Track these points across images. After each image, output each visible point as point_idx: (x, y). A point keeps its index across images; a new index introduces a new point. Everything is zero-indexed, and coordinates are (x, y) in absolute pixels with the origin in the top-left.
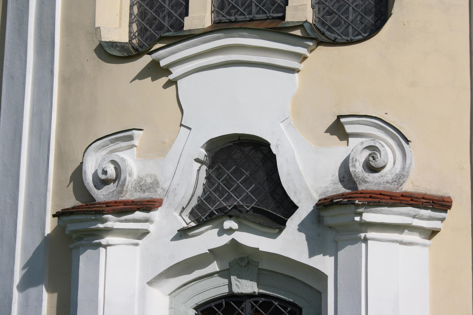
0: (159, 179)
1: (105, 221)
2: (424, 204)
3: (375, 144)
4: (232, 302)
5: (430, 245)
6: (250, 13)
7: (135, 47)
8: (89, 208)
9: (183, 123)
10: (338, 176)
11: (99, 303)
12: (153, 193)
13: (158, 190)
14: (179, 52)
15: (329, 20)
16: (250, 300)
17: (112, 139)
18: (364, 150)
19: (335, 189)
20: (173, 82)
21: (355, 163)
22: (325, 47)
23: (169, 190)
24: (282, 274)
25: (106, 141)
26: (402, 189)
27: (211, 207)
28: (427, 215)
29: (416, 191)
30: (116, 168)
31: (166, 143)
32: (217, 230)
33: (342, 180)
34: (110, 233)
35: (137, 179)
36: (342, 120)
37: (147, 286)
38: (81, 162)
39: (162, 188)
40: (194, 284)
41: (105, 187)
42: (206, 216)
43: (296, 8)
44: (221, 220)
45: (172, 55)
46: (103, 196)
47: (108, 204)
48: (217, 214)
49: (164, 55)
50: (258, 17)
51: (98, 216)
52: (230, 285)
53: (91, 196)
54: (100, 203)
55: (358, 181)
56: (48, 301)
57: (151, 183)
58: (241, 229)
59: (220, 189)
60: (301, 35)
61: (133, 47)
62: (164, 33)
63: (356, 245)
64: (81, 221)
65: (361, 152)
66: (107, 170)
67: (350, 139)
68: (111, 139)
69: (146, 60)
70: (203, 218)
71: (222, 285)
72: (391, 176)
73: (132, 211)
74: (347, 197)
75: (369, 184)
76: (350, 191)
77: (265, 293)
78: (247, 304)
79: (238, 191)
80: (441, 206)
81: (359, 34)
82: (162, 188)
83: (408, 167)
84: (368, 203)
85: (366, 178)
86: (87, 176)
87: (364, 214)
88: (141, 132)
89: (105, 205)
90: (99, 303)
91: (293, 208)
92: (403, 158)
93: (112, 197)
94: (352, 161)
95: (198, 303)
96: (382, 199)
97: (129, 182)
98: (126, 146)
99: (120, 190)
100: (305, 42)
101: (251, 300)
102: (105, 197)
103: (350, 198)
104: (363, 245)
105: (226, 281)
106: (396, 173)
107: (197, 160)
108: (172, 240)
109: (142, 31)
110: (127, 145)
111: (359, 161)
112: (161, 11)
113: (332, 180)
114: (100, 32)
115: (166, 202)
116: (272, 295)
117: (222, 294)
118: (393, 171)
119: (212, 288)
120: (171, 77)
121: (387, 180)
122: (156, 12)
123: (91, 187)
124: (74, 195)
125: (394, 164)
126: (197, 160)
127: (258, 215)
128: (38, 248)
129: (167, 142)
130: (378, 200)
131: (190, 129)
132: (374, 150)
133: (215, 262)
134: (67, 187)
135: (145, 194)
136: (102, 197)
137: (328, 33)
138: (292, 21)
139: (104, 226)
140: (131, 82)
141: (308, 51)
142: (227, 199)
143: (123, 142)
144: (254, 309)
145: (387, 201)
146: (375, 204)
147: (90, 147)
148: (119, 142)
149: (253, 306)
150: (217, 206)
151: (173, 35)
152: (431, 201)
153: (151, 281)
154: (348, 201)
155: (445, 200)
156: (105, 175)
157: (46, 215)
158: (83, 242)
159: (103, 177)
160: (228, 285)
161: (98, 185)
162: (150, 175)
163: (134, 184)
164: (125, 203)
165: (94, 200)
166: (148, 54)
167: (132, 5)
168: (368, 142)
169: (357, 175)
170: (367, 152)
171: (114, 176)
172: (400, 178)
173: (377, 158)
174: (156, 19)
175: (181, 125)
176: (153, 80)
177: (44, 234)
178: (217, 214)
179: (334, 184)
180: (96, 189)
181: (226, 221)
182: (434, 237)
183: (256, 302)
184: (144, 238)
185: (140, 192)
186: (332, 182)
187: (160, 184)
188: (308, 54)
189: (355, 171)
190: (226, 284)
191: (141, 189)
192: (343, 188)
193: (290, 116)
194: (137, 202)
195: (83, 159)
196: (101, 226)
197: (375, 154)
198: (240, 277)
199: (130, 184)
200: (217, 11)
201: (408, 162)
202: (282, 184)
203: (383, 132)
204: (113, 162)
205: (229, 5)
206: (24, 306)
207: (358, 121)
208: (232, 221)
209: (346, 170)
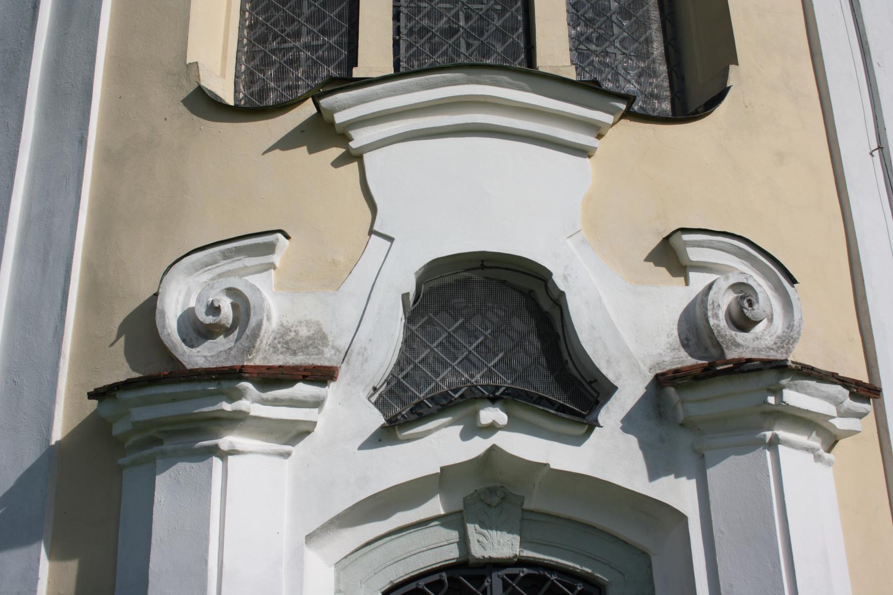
0: (326, 330)
1: (240, 395)
3: (747, 281)
4: (463, 577)
9: (376, 228)
10: (678, 336)
11: (209, 578)
13: (326, 350)
14: (375, 100)
16: (500, 573)
17: (229, 249)
19: (677, 358)
21: (717, 311)
22: (632, 122)
23: (351, 350)
24: (569, 520)
25: (215, 253)
31: (339, 264)
33: (685, 343)
34: (238, 426)
35: (279, 329)
38: (154, 292)
39: (333, 347)
40: (387, 542)
41: (206, 343)
45: (359, 104)
46: (203, 359)
49: (346, 102)
51: (225, 385)
52: (464, 543)
55: (725, 343)
56: (49, 582)
57: (309, 338)
58: (514, 425)
63: (750, 455)
64: (174, 399)
66: (219, 306)
67: (692, 275)
68: (225, 250)
71: (446, 543)
72: (771, 339)
74: (679, 379)
75: (743, 349)
77: (535, 558)
78: (495, 582)
80: (868, 390)
82: (335, 346)
83: (798, 325)
84: (801, 367)
86: (167, 321)
90: (209, 578)
92: (784, 310)
93: (227, 359)
94: (712, 307)
95: (394, 580)
97: (265, 333)
98: (256, 265)
99: (247, 347)
100: (613, 103)
101: (503, 573)
102: (210, 361)
105: (454, 535)
106: (777, 334)
108: (362, 447)
113: (669, 343)
114: (198, 71)
115: (346, 372)
116: (548, 562)
117: (446, 561)
119: (424, 549)
121: (766, 345)
123: (175, 341)
128: (30, 473)
129: (342, 261)
131: (391, 239)
134: (112, 345)
135: (297, 358)
139: (232, 408)
143: (250, 256)
144: (510, 589)
147: (177, 264)
148: (242, 257)
150: (430, 392)
156: (213, 316)
157: (55, 404)
159: (209, 320)
160: (458, 543)
161: (191, 339)
162: (307, 321)
163: (271, 338)
172: (788, 343)
175: (372, 232)
179: (673, 350)
180: (186, 347)
181: (485, 409)
183: (513, 577)
184: (298, 443)
185: (284, 354)
186: (669, 346)
187: (330, 338)
190: (454, 541)
191: (288, 349)
192: (690, 358)
195: (159, 287)
196: (227, 407)
199: (266, 335)
201: (797, 316)
202: (583, 345)
203: (749, 265)
204: (231, 292)
207: (711, 242)
208: (498, 409)
209: (689, 328)
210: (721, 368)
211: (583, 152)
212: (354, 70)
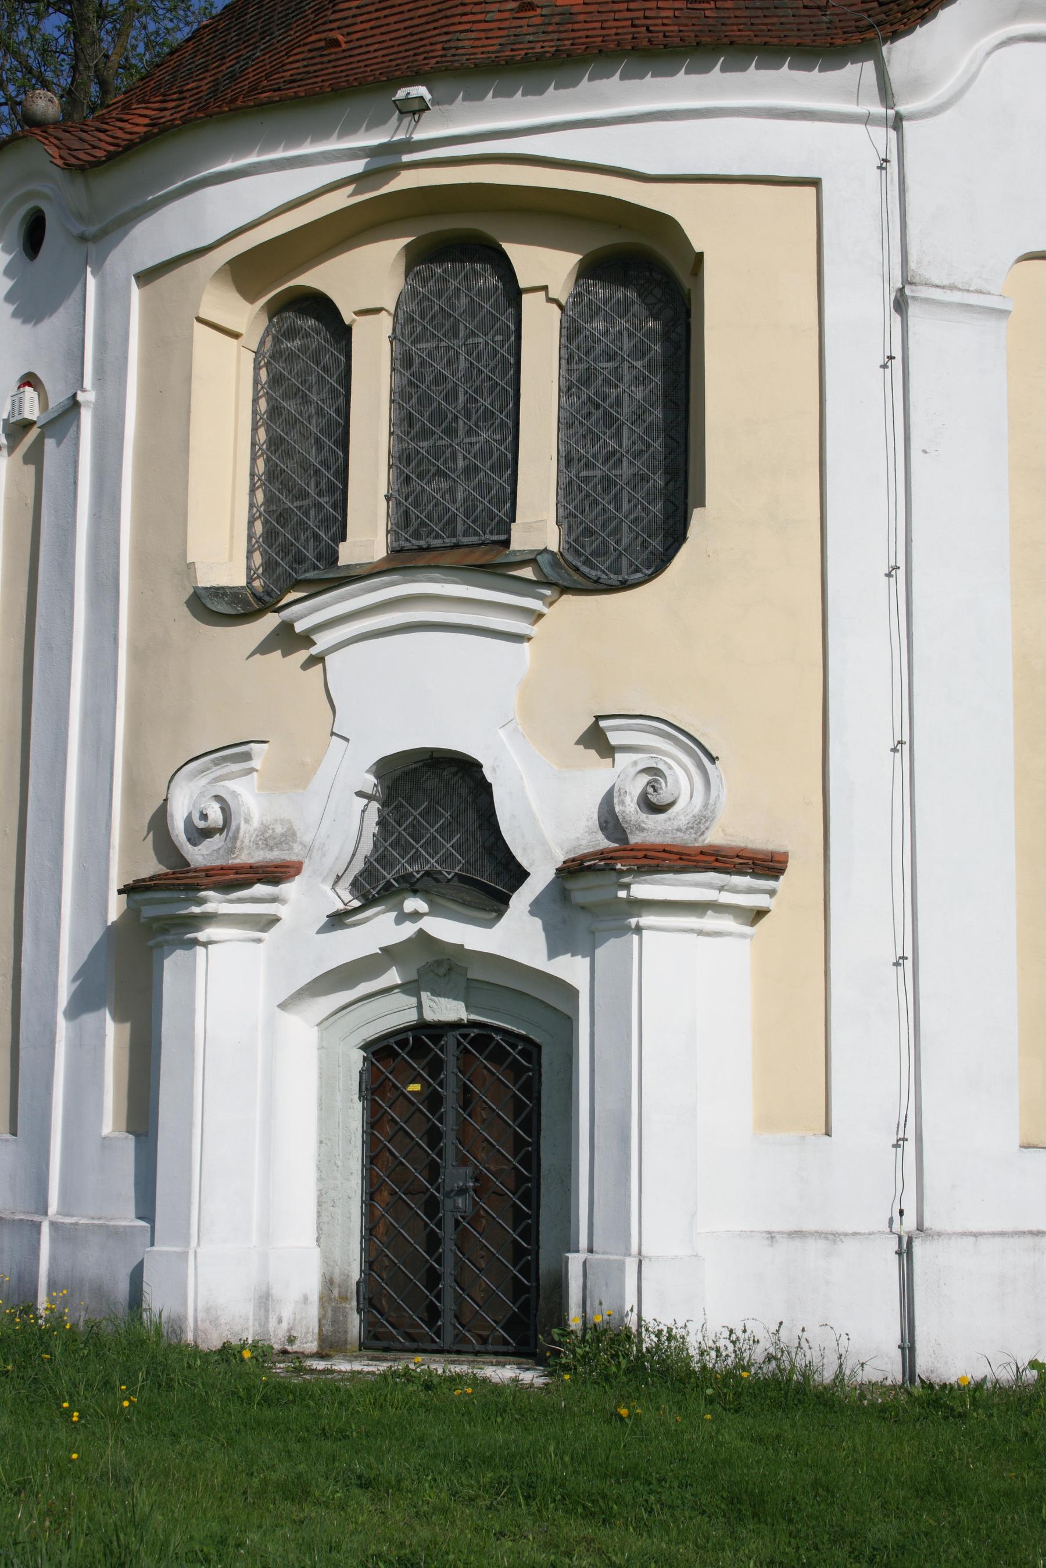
0: (296, 828)
1: (202, 902)
2: (737, 866)
5: (753, 936)
6: (453, 534)
7: (257, 594)
8: (177, 878)
9: (335, 731)
12: (287, 852)
13: (295, 846)
15: (590, 545)
18: (640, 775)
20: (318, 659)
24: (507, 987)
26: (704, 840)
27: (386, 874)
28: (744, 885)
29: (730, 843)
30: (223, 809)
32: (393, 915)
33: (603, 828)
36: (603, 724)
37: (278, 1011)
39: (301, 843)
42: (378, 889)
43: (528, 527)
44: (399, 898)
46: (202, 857)
47: (208, 872)
48: (397, 885)
50: (466, 540)
51: (191, 894)
52: (420, 1007)
53: (182, 857)
54: (196, 871)
57: (283, 835)
58: (435, 911)
59: (403, 842)
60: (535, 579)
61: (254, 595)
62: (306, 571)
64: (164, 902)
65: (634, 779)
69: (270, 621)
70: (374, 893)
73: (248, 884)
76: (616, 845)
78: (450, 1040)
79: (432, 845)
81: (637, 570)
85: (643, 822)
87: (632, 886)
88: (266, 744)
89: (203, 874)
91: (520, 875)
93: (217, 858)
96: (664, 860)
101: (457, 1033)
103: (611, 858)
104: (635, 938)
105: (414, 1001)
106: (694, 813)
107: (360, 794)
108: (319, 932)
109: (269, 565)
110: (241, 768)
111: (630, 793)
112: (301, 529)
113: (587, 826)
118: (689, 811)
120: (314, 651)
122: (496, 319)
124: (156, 854)
125: (691, 797)
126: (360, 794)
127: (466, 886)
130: (656, 862)
131: (347, 740)
132: (656, 775)
133: (394, 968)
136: (200, 858)
137: (585, 569)
138: (521, 549)
140: (247, 658)
141: (544, 604)
142: (412, 861)
144: (462, 1047)
145: (672, 863)
146: (651, 869)
149: (459, 1043)
151: (316, 577)
152: (750, 862)
153: (284, 1002)
154: (606, 864)
155: (776, 858)
158: (169, 937)
159: (201, 824)
162: (281, 820)
164: (237, 869)
165: (189, 865)
166: (274, 611)
167: (252, 519)
168: (644, 760)
169: (628, 818)
170: (645, 779)
171: (221, 823)
172: (700, 823)
173: (661, 788)
174: (292, 544)
175: (333, 734)
176: (285, 654)
177: (106, 922)
178: (397, 885)
182: (761, 922)
183: (464, 1036)
186: (587, 829)
187: (299, 835)
188: (545, 610)
189: (624, 812)
191: (267, 845)
192: (606, 840)
193: (517, 717)
194: (257, 867)
196: (196, 910)
197: (656, 781)
198: (435, 993)
199: (247, 835)
200: (395, 531)
204: (218, 798)
205: (416, 519)
206: (76, 1045)
210: (588, 863)
211: (519, 638)
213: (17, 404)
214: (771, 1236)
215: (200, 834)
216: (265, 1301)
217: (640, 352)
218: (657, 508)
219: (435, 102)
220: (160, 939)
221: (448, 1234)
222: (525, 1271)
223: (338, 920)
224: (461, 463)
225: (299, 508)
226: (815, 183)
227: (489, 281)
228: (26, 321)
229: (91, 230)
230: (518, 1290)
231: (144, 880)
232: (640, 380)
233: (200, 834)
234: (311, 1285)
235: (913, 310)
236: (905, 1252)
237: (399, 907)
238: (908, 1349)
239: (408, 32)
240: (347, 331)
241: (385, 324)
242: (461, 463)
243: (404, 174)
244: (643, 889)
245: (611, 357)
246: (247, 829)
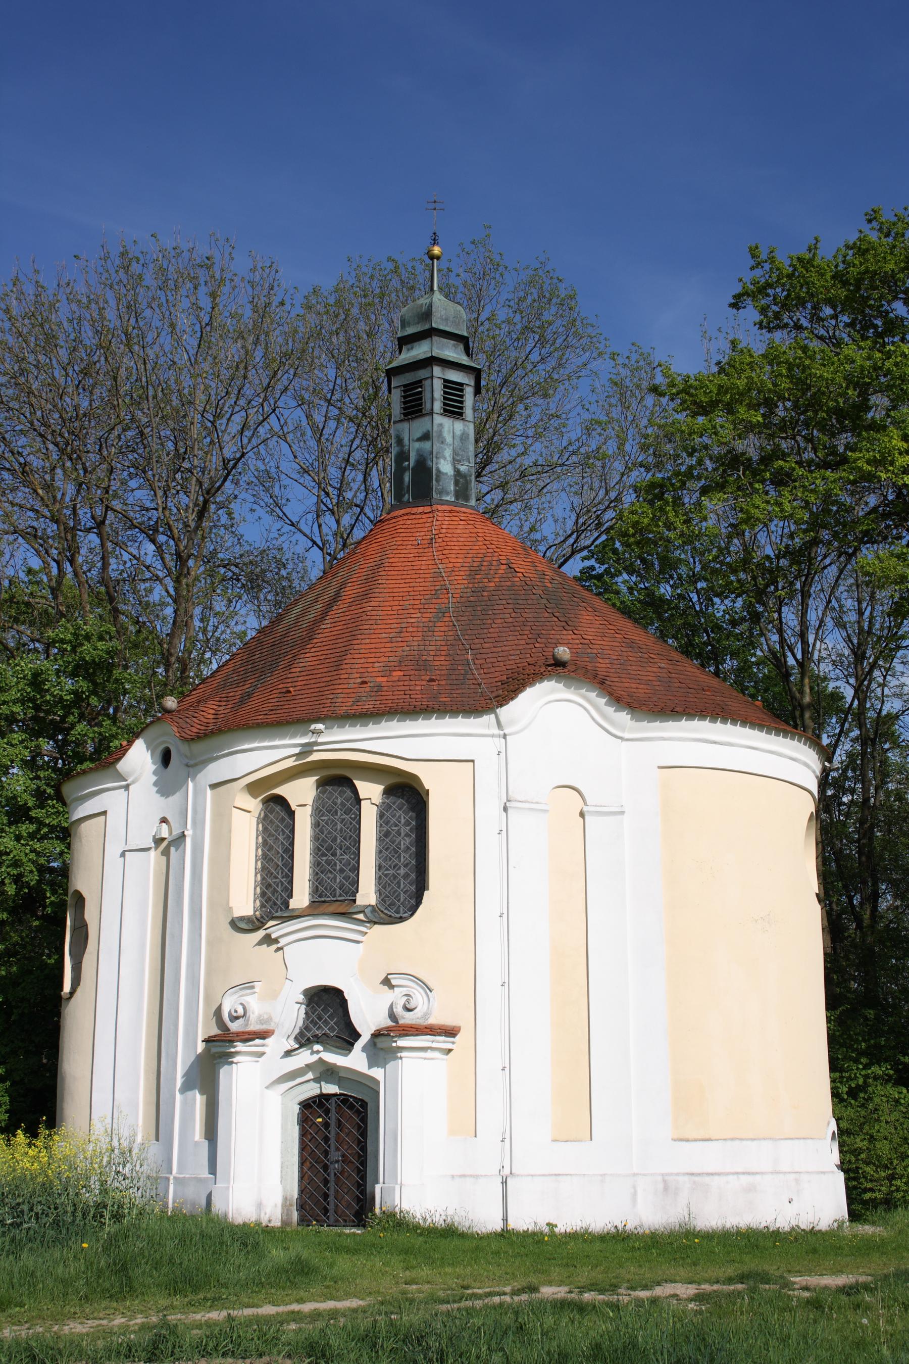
1: (235, 1047)
6: (335, 896)
47: (238, 1034)
52: (321, 1088)
58: (325, 1050)
64: (220, 1046)
69: (261, 934)
78: (333, 1101)
91: (357, 1036)
107: (297, 1003)
120: (279, 945)
126: (297, 1003)
142: (318, 1029)
159: (235, 1015)
164: (249, 1033)
168: (404, 991)
196: (233, 1050)
204: (242, 1004)
206: (184, 1103)
211: (358, 942)
212: (291, 901)
213: (159, 830)
214: (453, 1176)
215: (234, 1018)
216: (260, 1206)
217: (407, 824)
218: (413, 888)
219: (326, 728)
220: (219, 1060)
221: (332, 1178)
222: (361, 1193)
223: (288, 1053)
224: (338, 868)
225: (275, 883)
226: (473, 761)
227: (349, 793)
228: (162, 795)
229: (192, 762)
230: (359, 1200)
231: (212, 1037)
232: (407, 835)
233: (234, 1018)
234: (279, 1201)
235: (510, 811)
236: (504, 1183)
237: (312, 1048)
238: (505, 1220)
239: (317, 690)
240: (294, 812)
241: (308, 810)
242: (338, 868)
243: (315, 753)
244: (402, 1042)
245: (396, 825)
246: (253, 1016)
